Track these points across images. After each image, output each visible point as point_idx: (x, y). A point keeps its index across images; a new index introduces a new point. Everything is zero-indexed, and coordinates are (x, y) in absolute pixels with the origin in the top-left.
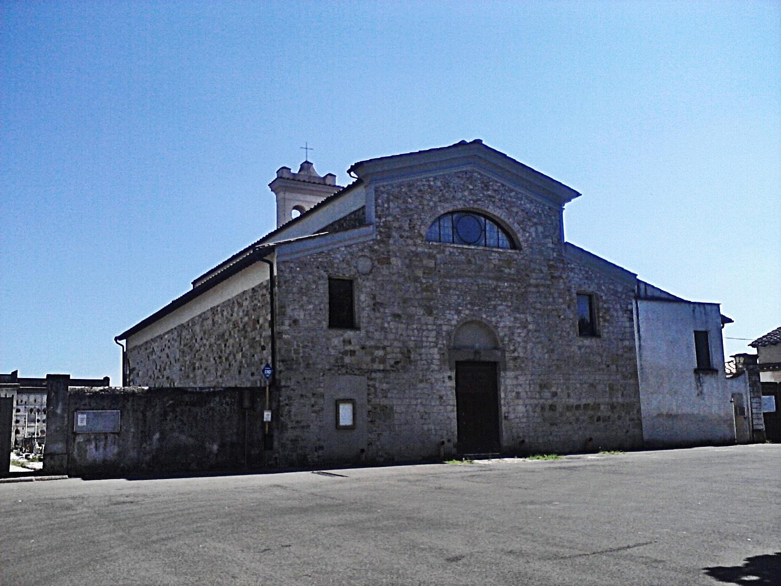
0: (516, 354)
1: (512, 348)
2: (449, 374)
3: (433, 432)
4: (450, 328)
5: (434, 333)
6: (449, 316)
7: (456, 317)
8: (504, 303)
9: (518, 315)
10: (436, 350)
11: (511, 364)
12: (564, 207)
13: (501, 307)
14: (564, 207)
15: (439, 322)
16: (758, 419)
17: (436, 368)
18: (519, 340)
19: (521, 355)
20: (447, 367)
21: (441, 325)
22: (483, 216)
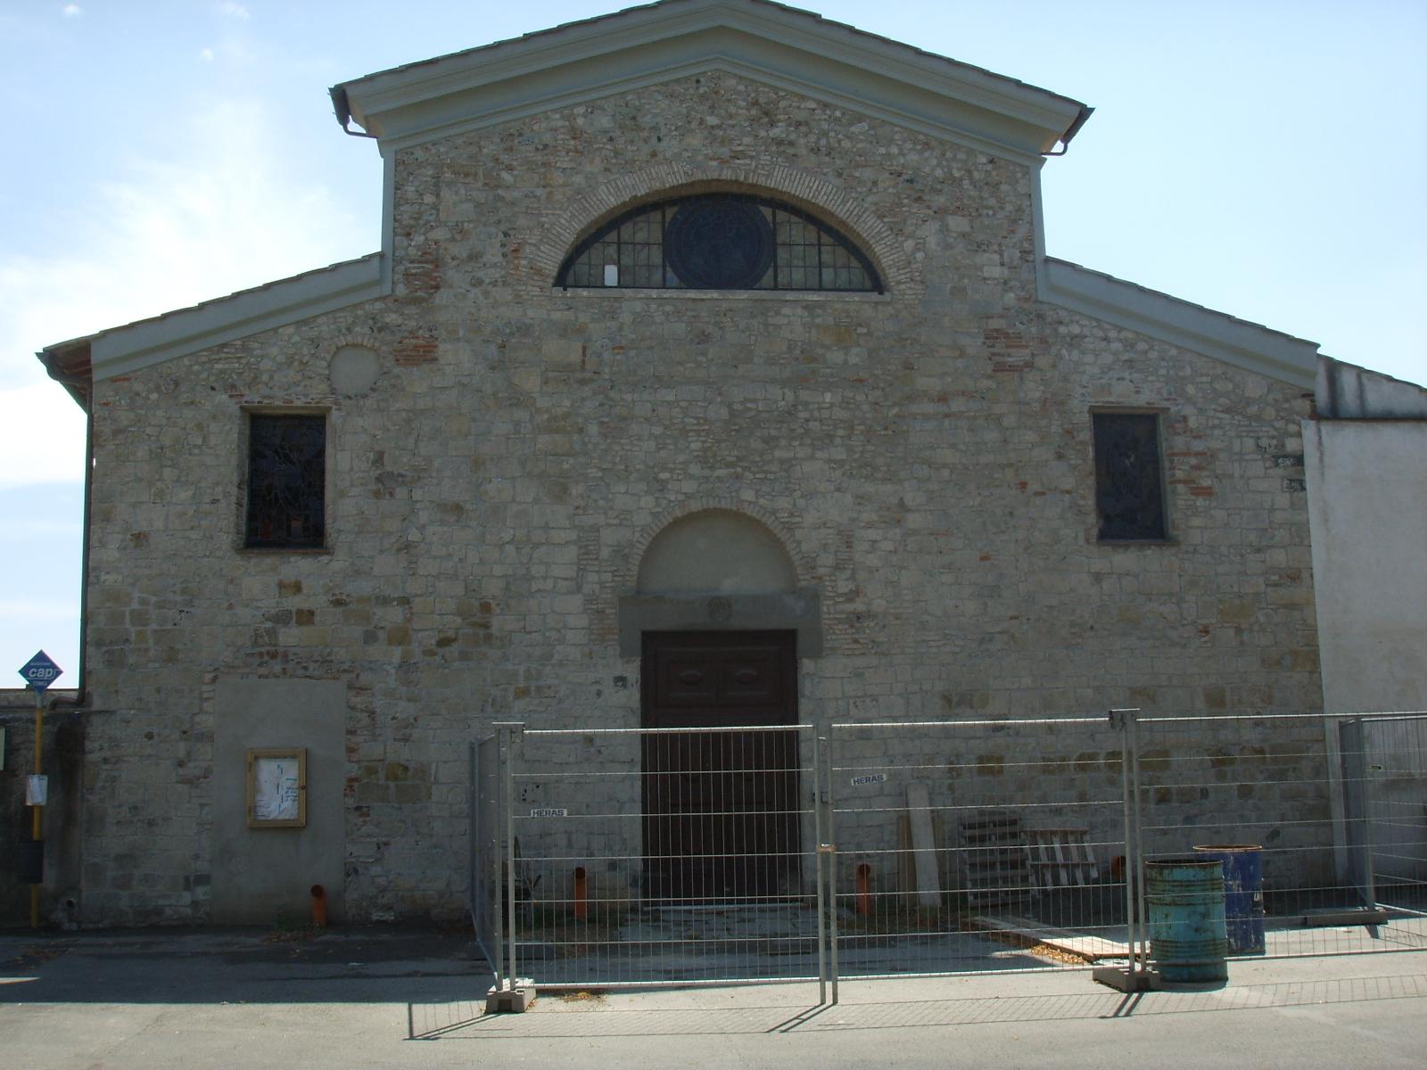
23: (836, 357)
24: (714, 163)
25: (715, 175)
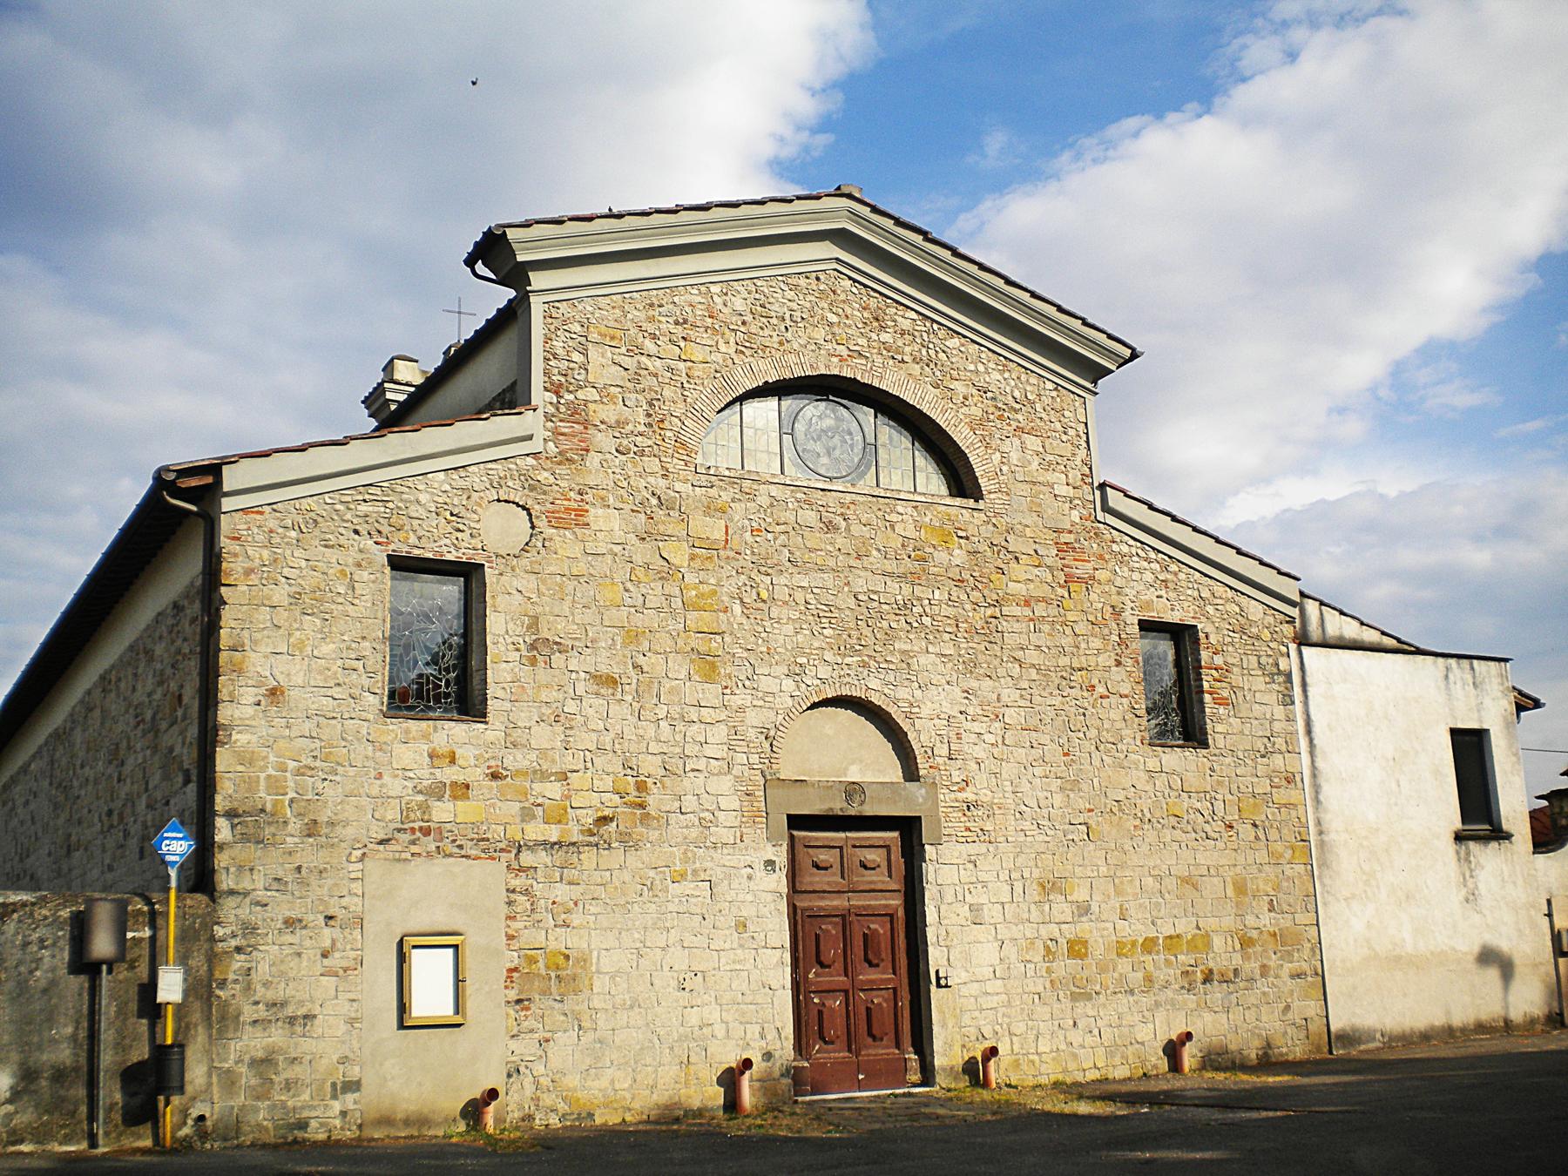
0: (969, 795)
2: (769, 852)
5: (721, 732)
6: (766, 684)
7: (789, 684)
9: (974, 684)
10: (725, 784)
11: (953, 823)
13: (923, 660)
15: (736, 701)
19: (986, 795)
21: (741, 709)
23: (941, 556)
24: (835, 360)
25: (836, 372)
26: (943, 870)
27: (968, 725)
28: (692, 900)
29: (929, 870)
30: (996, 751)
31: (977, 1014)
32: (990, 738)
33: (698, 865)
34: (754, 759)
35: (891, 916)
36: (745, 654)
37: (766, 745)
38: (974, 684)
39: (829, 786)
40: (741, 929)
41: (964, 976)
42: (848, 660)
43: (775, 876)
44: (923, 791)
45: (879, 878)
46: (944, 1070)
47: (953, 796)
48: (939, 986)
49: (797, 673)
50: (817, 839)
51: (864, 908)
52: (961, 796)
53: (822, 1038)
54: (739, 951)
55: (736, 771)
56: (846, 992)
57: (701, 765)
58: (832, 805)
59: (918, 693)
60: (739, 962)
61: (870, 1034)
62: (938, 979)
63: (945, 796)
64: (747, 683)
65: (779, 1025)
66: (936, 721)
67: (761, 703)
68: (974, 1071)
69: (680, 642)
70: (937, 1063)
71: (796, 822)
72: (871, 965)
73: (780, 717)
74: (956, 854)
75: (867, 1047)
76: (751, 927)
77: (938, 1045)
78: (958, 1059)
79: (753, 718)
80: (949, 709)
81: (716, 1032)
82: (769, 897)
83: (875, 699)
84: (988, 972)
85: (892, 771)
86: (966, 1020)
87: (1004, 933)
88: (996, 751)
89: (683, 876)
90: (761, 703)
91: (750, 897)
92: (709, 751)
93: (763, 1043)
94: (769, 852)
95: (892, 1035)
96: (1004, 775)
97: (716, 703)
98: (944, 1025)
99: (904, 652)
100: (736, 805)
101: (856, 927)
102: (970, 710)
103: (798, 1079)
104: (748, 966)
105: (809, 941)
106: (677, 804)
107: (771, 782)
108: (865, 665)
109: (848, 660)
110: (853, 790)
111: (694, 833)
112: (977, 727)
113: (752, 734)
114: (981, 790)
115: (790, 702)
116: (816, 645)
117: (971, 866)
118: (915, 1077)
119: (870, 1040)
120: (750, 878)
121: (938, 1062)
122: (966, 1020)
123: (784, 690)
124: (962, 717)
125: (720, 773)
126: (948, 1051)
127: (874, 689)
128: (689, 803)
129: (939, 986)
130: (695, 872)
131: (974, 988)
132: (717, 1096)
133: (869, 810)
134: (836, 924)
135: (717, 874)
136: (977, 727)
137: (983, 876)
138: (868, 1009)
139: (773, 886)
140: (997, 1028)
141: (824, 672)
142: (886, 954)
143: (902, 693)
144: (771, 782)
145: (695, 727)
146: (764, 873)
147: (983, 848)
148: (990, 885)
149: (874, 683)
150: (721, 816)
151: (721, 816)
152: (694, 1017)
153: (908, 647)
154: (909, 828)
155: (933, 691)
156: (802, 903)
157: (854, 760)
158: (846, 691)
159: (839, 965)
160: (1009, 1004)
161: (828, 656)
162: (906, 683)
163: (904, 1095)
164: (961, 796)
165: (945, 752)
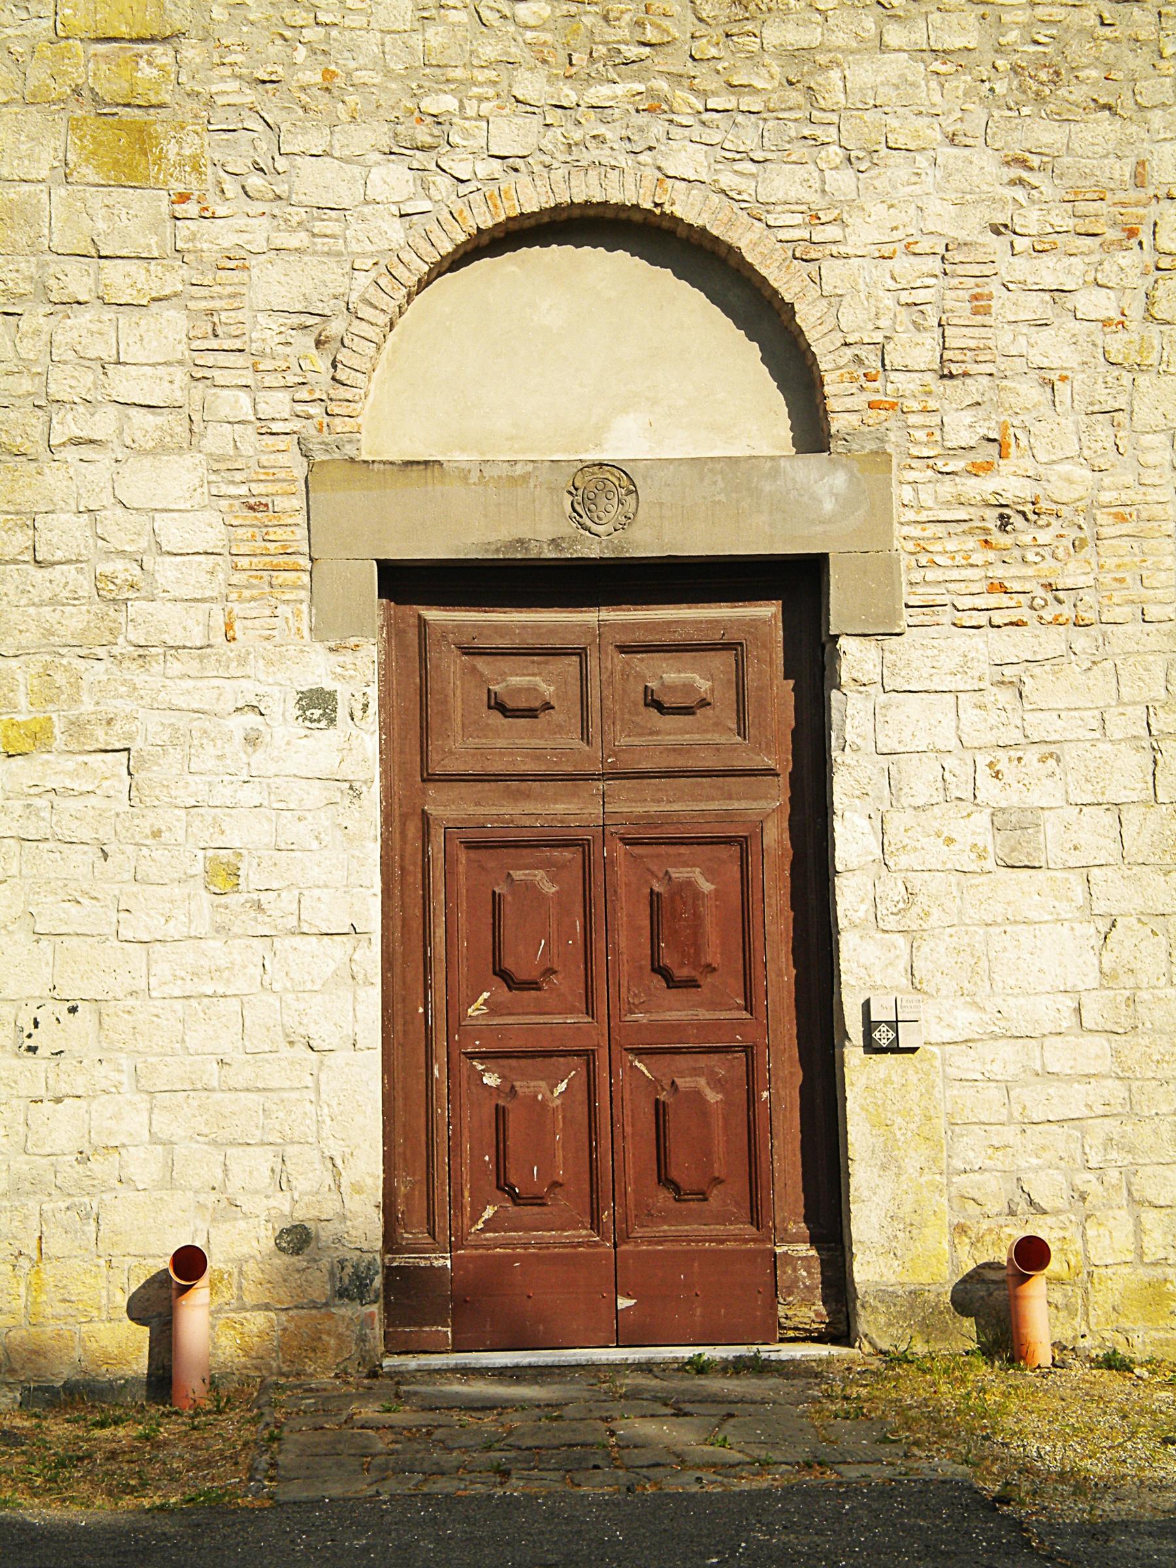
0: (1008, 483)
1: (963, 428)
2: (318, 668)
3: (143, 1165)
4: (334, 276)
5: (169, 330)
6: (316, 181)
7: (393, 181)
8: (895, 35)
9: (1048, 135)
10: (180, 478)
11: (955, 568)
12: (791, 683)
13: (864, 74)
14: (791, 683)
15: (219, 237)
16: (118, 1071)
17: (188, 626)
18: (1053, 348)
19: (1069, 482)
20: (295, 614)
21: (235, 261)
22: (599, 1219)
26: (903, 720)
27: (1021, 269)
28: (73, 804)
29: (852, 715)
30: (1116, 344)
31: (1009, 1134)
32: (1101, 304)
33: (87, 706)
34: (277, 404)
35: (742, 843)
36: (250, 96)
37: (322, 363)
38: (1048, 135)
39: (515, 479)
40: (220, 885)
41: (965, 1021)
42: (600, 93)
43: (330, 738)
44: (839, 480)
45: (707, 738)
46: (886, 1296)
47: (947, 488)
48: (871, 1047)
49: (419, 143)
50: (499, 630)
51: (649, 821)
52: (985, 486)
53: (504, 1186)
54: (214, 945)
55: (216, 439)
56: (588, 1055)
57: (103, 424)
58: (524, 532)
59: (843, 181)
60: (215, 973)
61: (665, 1180)
62: (869, 1026)
63: (916, 494)
64: (255, 182)
65: (334, 1148)
66: (903, 264)
67: (300, 239)
68: (991, 1302)
69: (38, 74)
70: (858, 1277)
71: (403, 582)
72: (672, 982)
73: (363, 280)
74: (950, 662)
75: (649, 1216)
76: (252, 877)
77: (865, 1222)
78: (940, 1265)
79: (274, 285)
80: (943, 219)
81: (132, 1170)
82: (316, 793)
83: (689, 208)
84: (1052, 1012)
85: (760, 417)
86: (970, 1149)
87: (1116, 892)
88: (1116, 344)
89: (39, 737)
90: (300, 239)
91: (250, 795)
92: (125, 385)
93: (282, 1203)
94: (318, 668)
95: (739, 1185)
96: (1145, 415)
97: (151, 243)
98: (889, 1164)
99: (795, 54)
100: (212, 535)
101: (623, 873)
102: (1031, 221)
103: (408, 1296)
104: (240, 985)
105: (461, 915)
106: (22, 539)
107: (331, 469)
108: (656, 106)
109: (600, 93)
110: (599, 484)
111: (75, 620)
112: (1049, 271)
113: (266, 333)
114: (1056, 460)
115: (396, 232)
116: (489, 51)
117: (1006, 697)
118: (809, 1311)
119: (664, 1197)
120: (252, 740)
121: (867, 1270)
122: (970, 1149)
123: (390, 207)
124: (997, 244)
125: (161, 449)
126: (906, 1232)
127: (686, 179)
128: (63, 533)
129: (871, 1047)
130: (77, 727)
131: (1005, 1058)
132: (126, 1347)
133: (646, 542)
134: (555, 871)
135: (148, 729)
136: (1049, 271)
137: (1043, 726)
138: (660, 1109)
139: (326, 763)
140: (1086, 1180)
141: (511, 134)
142: (716, 945)
143: (784, 184)
144: (331, 469)
145: (83, 319)
146: (299, 728)
147: (1052, 641)
148: (1070, 754)
149: (686, 160)
150: (166, 571)
151: (166, 571)
152: (61, 1129)
153: (810, 36)
154: (797, 582)
155: (897, 168)
156: (448, 807)
157: (638, 405)
158: (586, 189)
159: (567, 983)
160: (1131, 1112)
161: (531, 85)
162: (800, 151)
163: (737, 1367)
164: (985, 486)
165: (925, 353)
